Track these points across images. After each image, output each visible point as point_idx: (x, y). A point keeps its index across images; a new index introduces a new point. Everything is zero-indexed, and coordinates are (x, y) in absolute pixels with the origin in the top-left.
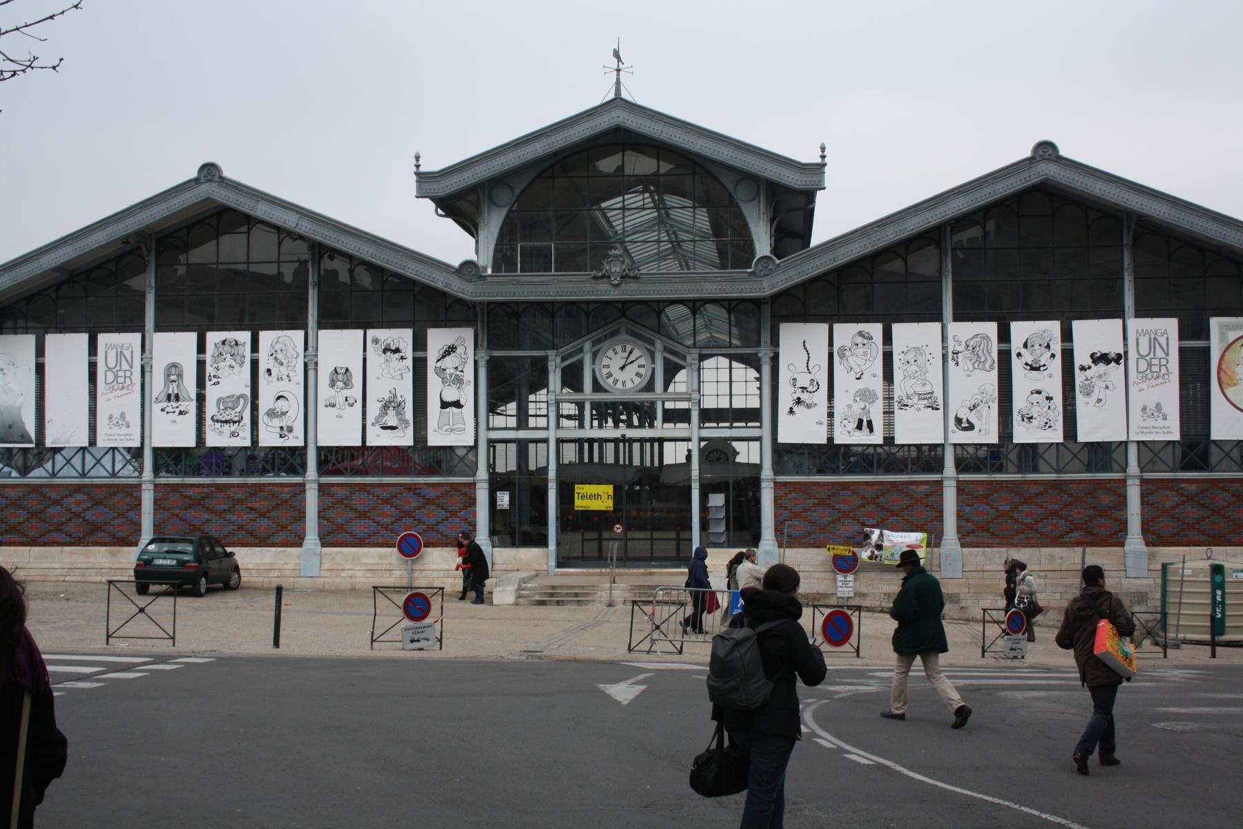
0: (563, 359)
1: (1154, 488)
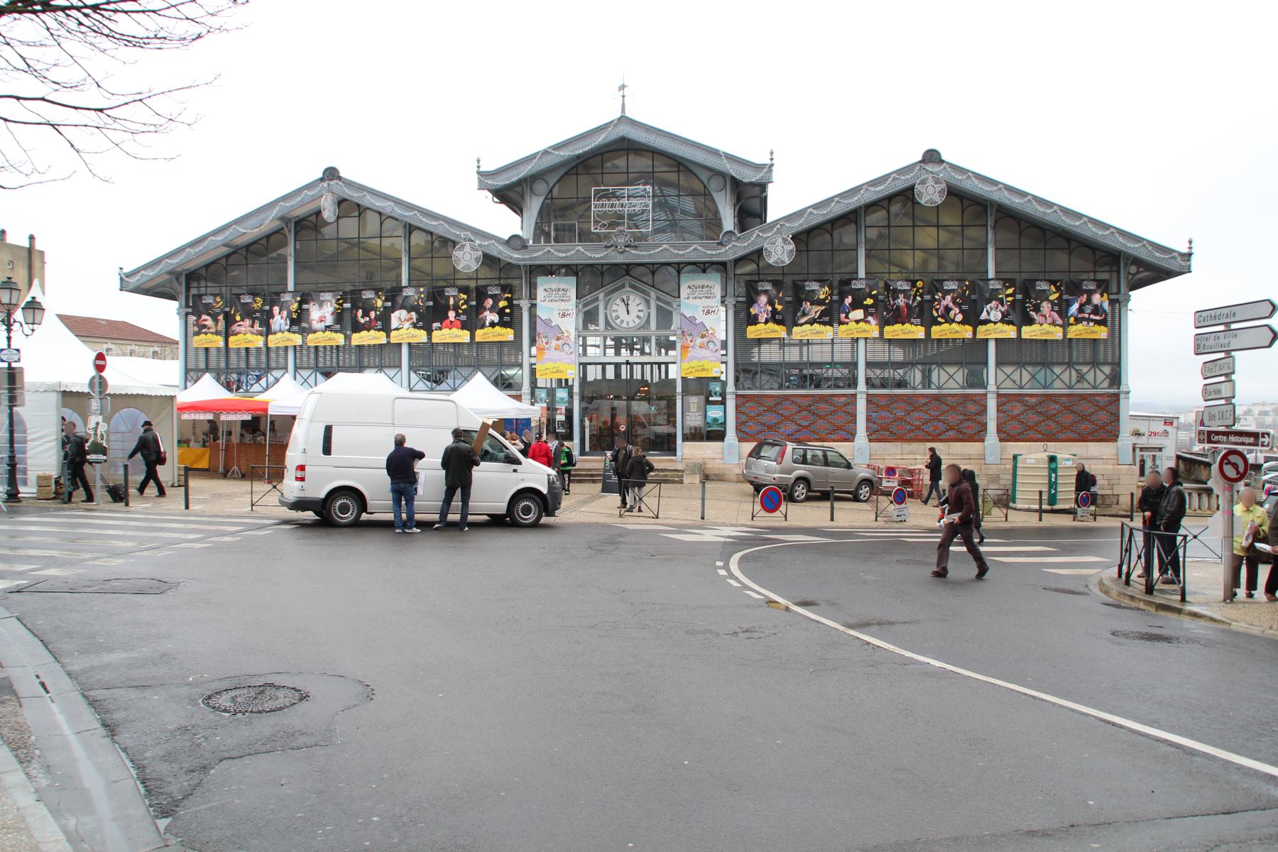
0: (585, 306)
1: (1006, 400)
